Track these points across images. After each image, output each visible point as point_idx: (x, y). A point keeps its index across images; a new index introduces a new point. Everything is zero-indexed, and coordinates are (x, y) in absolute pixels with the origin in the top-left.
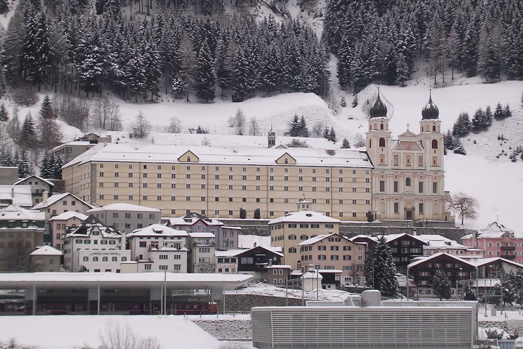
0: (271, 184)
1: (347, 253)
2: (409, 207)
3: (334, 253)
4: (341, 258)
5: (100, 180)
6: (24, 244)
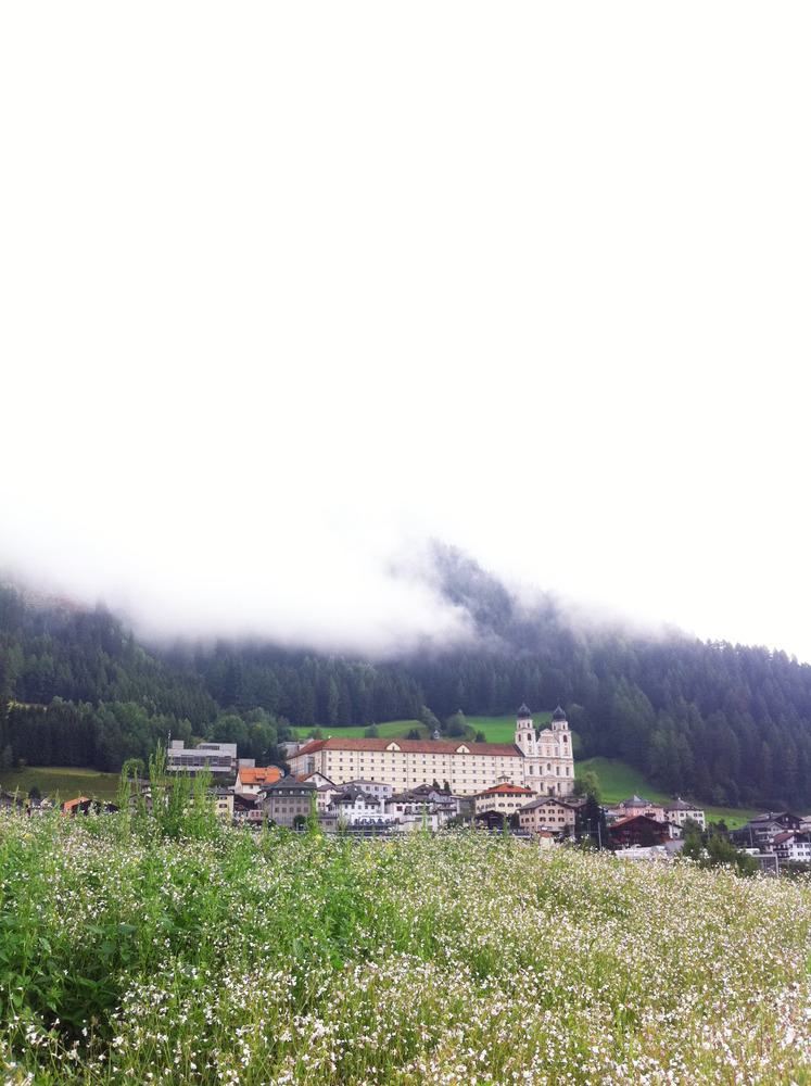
0: (453, 768)
1: (561, 815)
2: (551, 786)
3: (552, 815)
4: (557, 820)
5: (328, 764)
6: (591, 676)
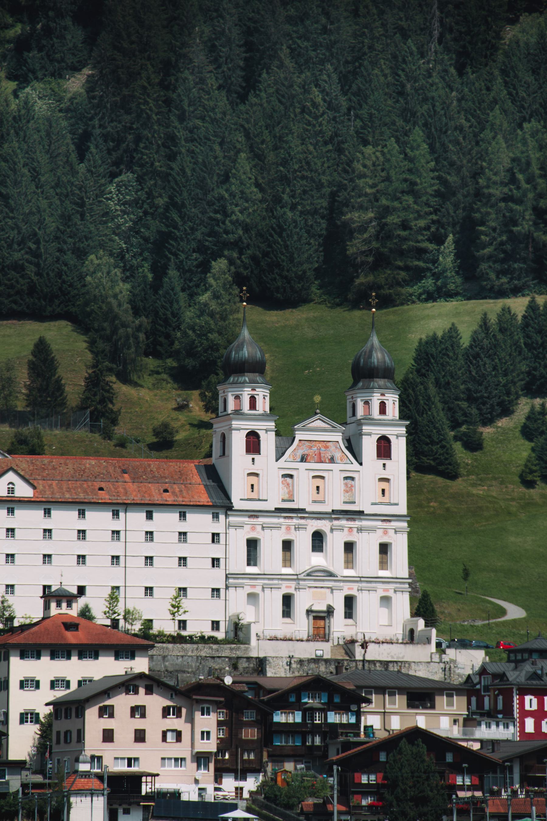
1: (173, 723)
